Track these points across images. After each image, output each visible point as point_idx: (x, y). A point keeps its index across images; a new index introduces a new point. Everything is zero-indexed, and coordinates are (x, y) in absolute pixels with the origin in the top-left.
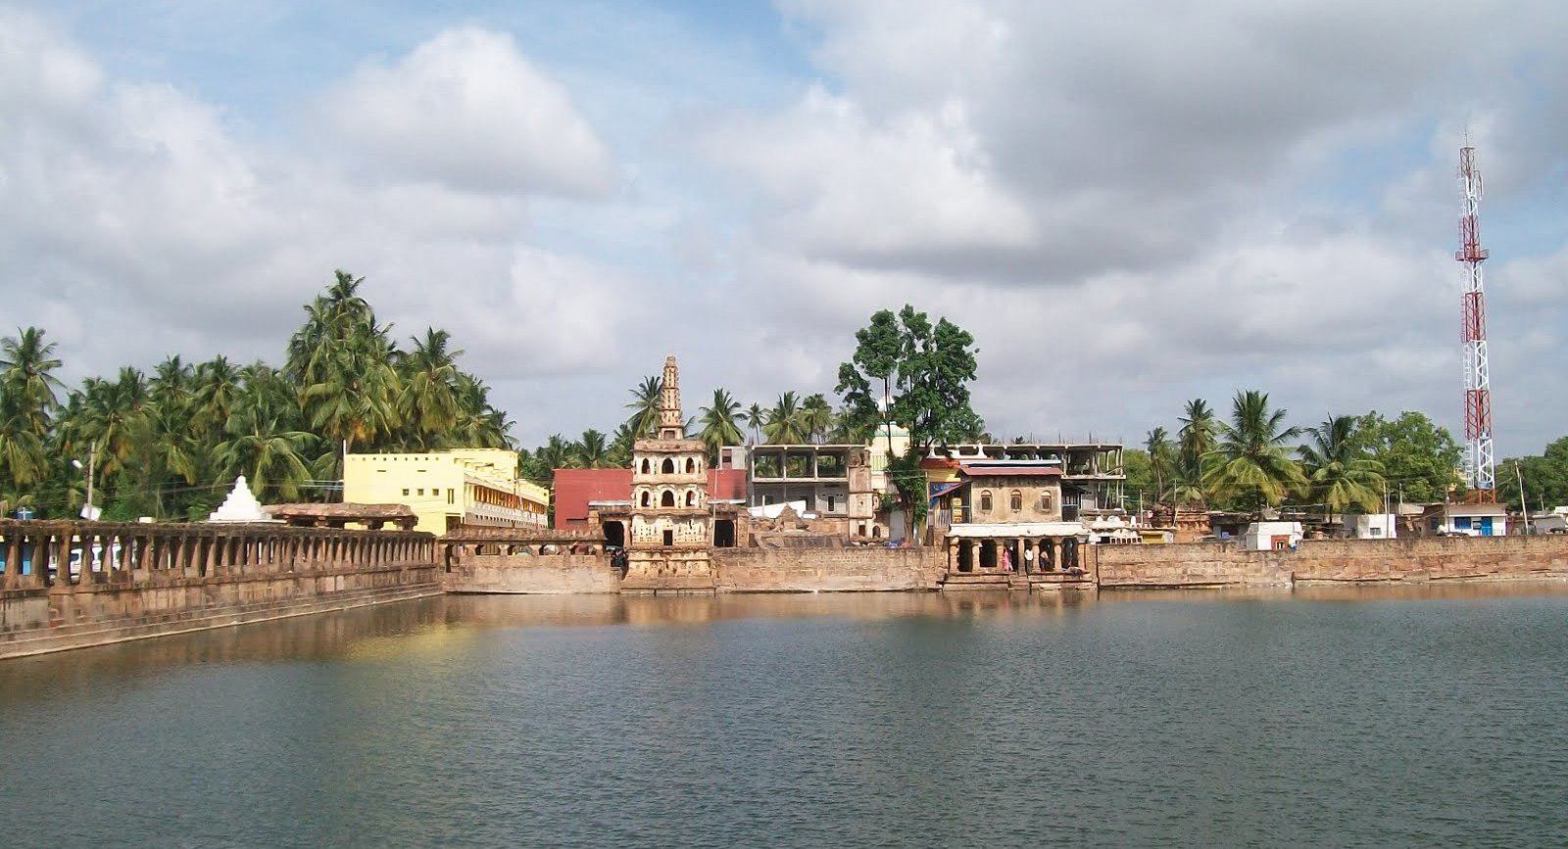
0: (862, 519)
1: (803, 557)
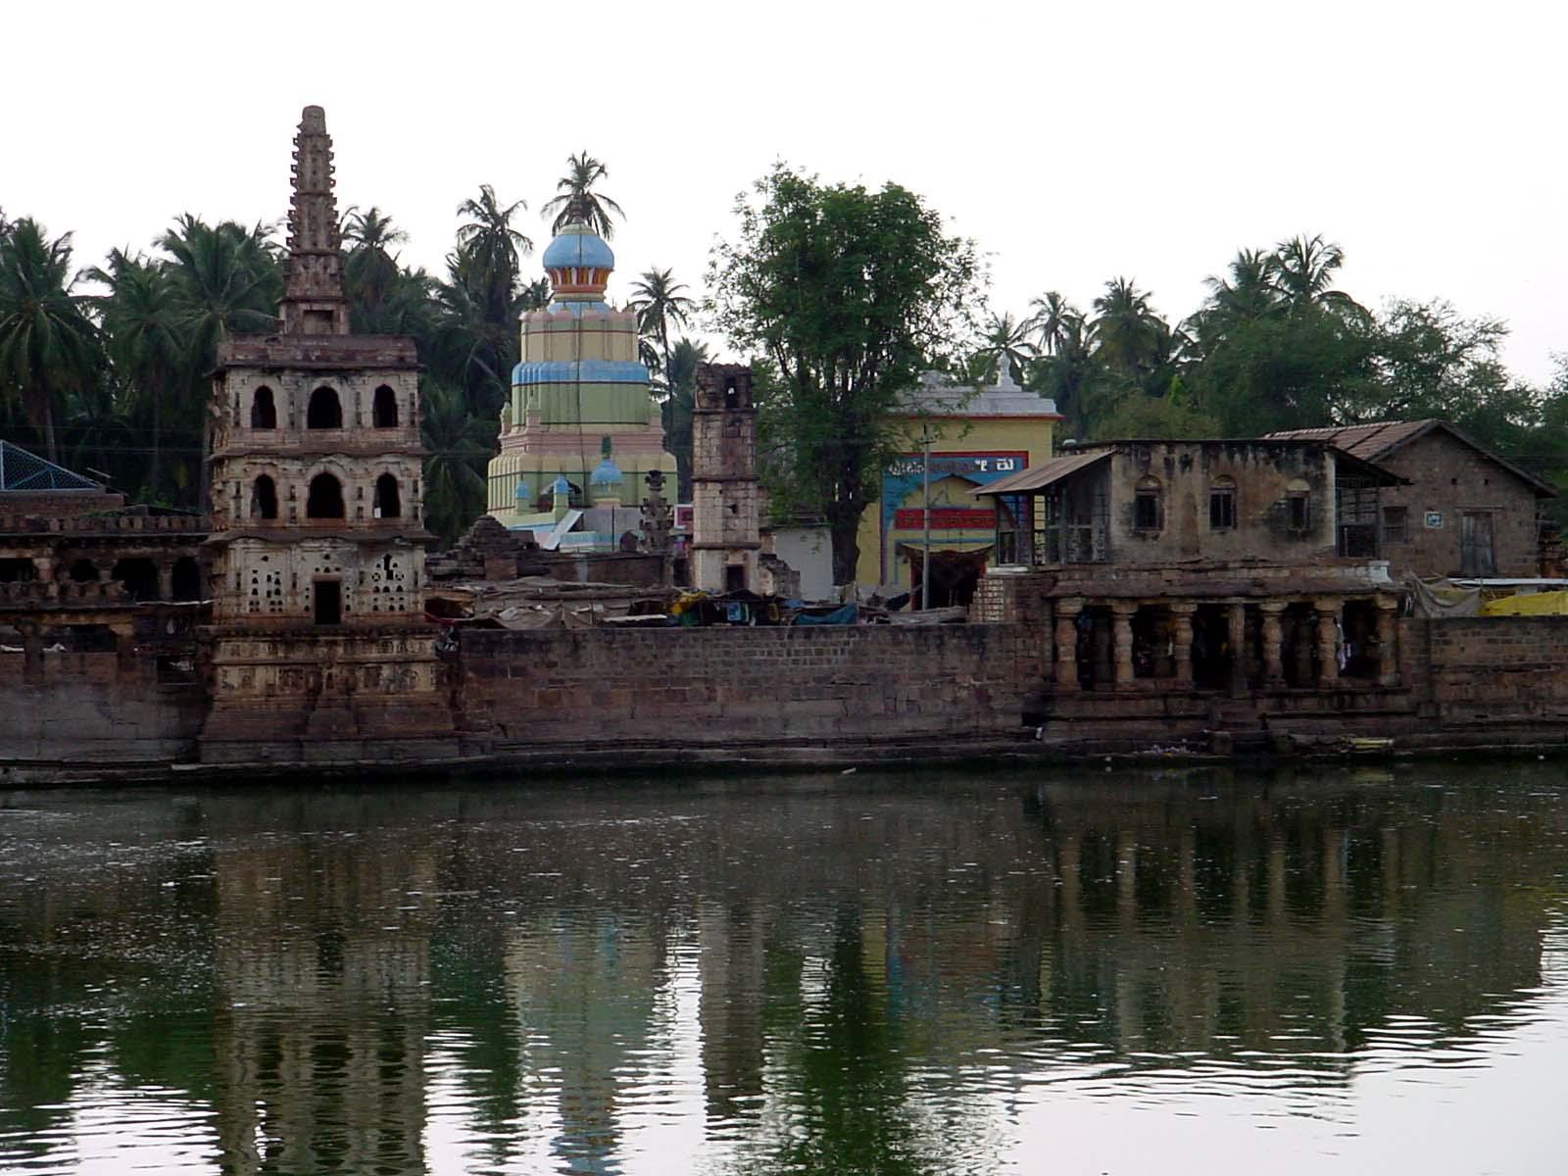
0: (736, 548)
1: (678, 651)
